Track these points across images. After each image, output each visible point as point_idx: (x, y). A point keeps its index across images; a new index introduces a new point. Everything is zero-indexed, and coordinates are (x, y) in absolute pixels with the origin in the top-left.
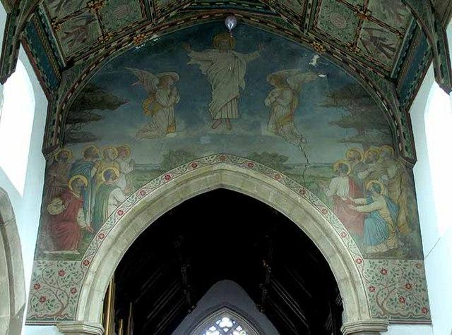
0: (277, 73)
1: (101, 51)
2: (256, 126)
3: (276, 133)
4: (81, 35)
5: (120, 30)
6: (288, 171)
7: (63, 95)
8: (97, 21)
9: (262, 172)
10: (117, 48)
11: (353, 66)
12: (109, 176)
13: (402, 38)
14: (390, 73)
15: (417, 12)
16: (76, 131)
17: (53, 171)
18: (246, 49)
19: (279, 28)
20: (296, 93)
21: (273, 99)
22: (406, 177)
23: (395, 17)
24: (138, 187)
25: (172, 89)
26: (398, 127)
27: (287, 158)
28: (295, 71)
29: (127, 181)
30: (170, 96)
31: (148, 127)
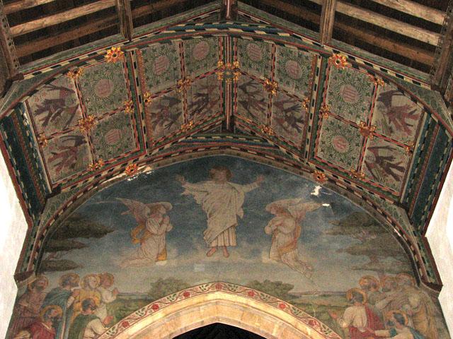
0: (276, 202)
1: (91, 179)
2: (256, 253)
3: (278, 261)
4: (69, 158)
5: (112, 159)
6: (294, 300)
7: (45, 221)
8: (88, 144)
9: (264, 300)
10: (107, 177)
11: (359, 193)
12: (88, 305)
13: (412, 152)
14: (399, 197)
15: (429, 106)
16: (55, 260)
17: (25, 301)
18: (244, 181)
19: (278, 160)
20: (298, 220)
21: (274, 227)
22: (432, 306)
23: (403, 128)
24: (120, 318)
25: (164, 218)
26: (415, 252)
27: (293, 286)
28: (298, 200)
29: (108, 311)
30: (161, 224)
31: (136, 255)
